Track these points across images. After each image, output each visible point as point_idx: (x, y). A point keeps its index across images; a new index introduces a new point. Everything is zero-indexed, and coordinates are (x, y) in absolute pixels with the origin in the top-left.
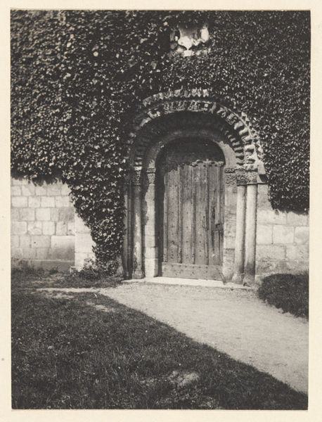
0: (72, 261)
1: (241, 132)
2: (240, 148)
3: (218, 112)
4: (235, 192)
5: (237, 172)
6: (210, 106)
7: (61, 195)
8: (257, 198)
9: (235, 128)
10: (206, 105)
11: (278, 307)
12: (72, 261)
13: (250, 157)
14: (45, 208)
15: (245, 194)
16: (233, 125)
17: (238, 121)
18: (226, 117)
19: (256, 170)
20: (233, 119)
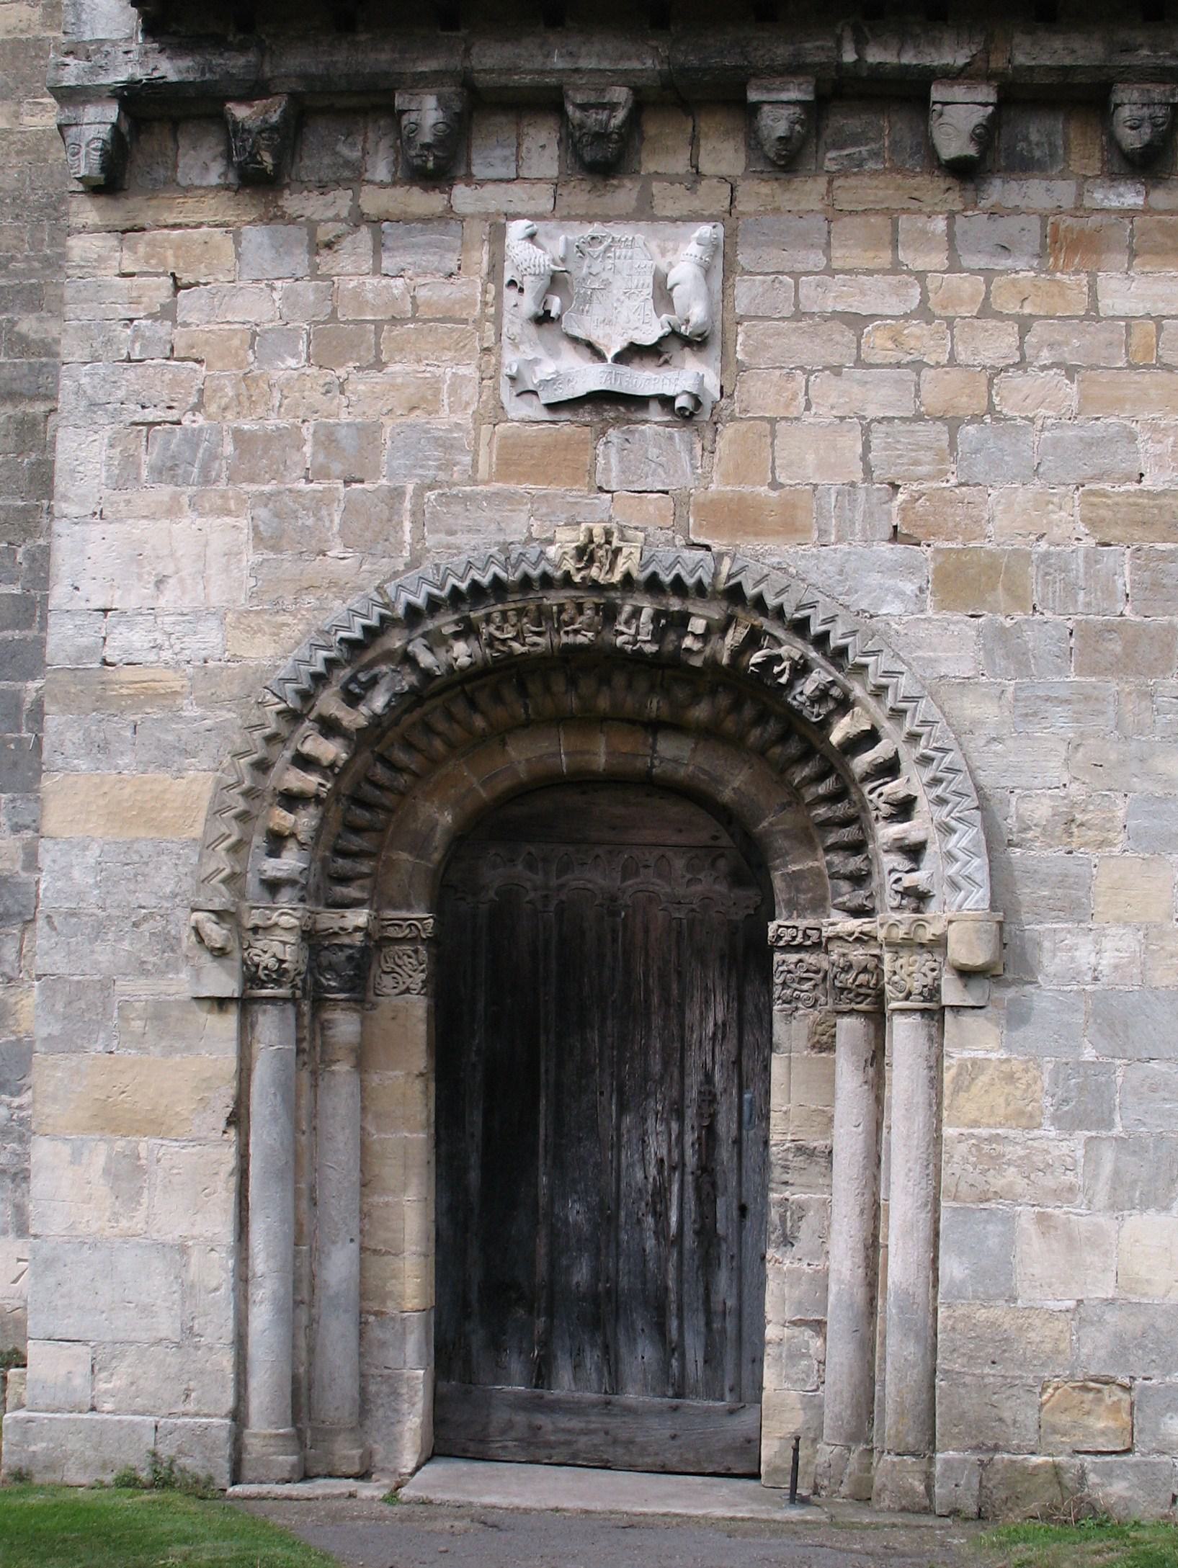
0: (31, 634)
1: (862, 762)
2: (847, 834)
3: (757, 657)
4: (825, 1044)
5: (836, 950)
6: (716, 630)
7: (799, 315)
8: (937, 1140)
9: (836, 737)
10: (698, 625)
11: (1026, 961)
12: (31, 634)
13: (908, 880)
14: (575, 340)
15: (876, 1058)
16: (825, 725)
17: (845, 705)
18: (790, 685)
19: (939, 943)
20: (822, 695)
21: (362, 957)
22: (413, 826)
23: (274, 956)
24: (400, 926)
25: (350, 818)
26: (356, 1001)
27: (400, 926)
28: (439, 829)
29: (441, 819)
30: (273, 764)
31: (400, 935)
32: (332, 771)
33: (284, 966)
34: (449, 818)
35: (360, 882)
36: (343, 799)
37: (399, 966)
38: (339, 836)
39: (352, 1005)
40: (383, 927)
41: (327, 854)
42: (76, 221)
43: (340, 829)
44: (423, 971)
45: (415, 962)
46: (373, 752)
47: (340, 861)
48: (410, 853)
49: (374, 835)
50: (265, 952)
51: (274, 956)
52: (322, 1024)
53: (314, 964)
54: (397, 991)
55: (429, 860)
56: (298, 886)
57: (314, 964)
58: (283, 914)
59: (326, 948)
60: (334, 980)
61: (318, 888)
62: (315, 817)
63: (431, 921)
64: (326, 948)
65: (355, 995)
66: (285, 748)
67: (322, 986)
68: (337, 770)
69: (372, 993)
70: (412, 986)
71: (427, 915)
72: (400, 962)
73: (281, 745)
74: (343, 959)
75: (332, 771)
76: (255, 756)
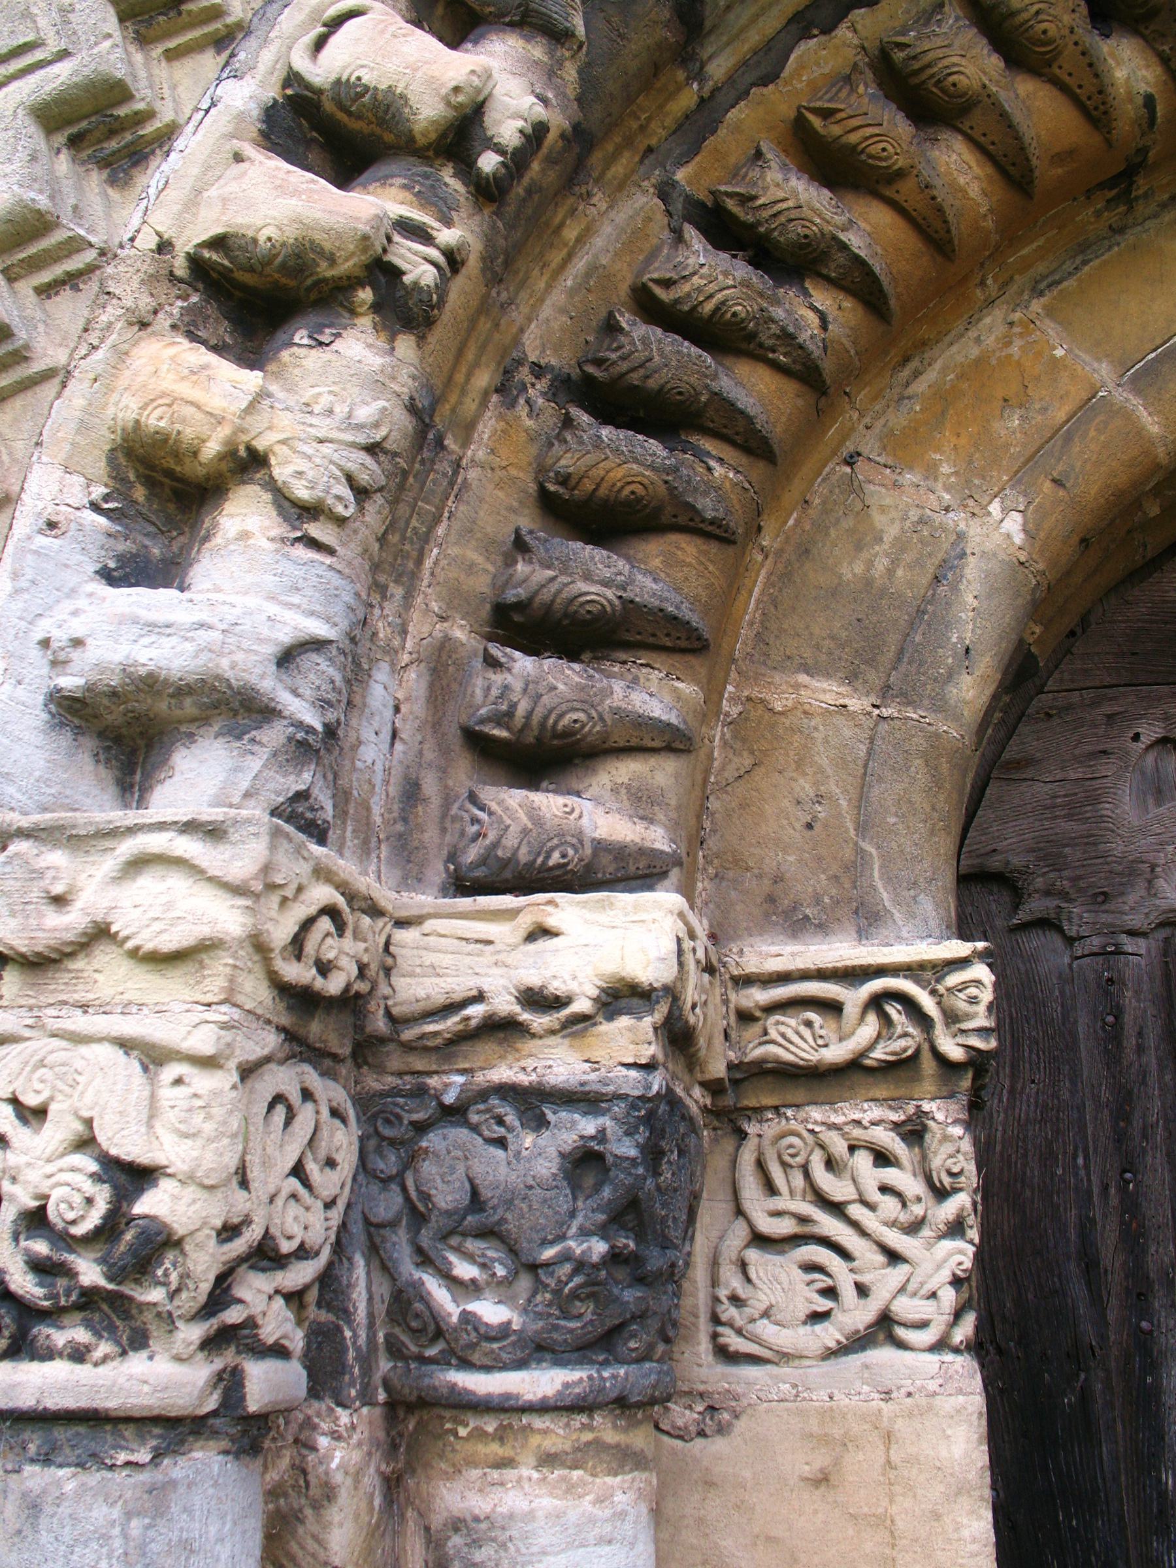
21: (653, 1155)
22: (852, 570)
23: (86, 1142)
24: (833, 1008)
25: (567, 462)
26: (622, 1405)
27: (833, 1008)
28: (972, 569)
29: (974, 531)
30: (169, 134)
31: (836, 1053)
32: (466, 166)
33: (150, 1204)
34: (1013, 525)
35: (626, 770)
36: (537, 391)
37: (836, 1208)
38: (520, 545)
39: (606, 1429)
40: (745, 1017)
41: (460, 633)
42: (297, 340)
43: (526, 521)
44: (956, 1228)
45: (912, 1185)
46: (665, 192)
47: (524, 664)
48: (851, 678)
49: (687, 548)
50: (39, 1114)
51: (86, 1142)
52: (434, 1541)
53: (388, 1204)
54: (829, 1334)
55: (940, 705)
56: (274, 735)
57: (388, 1204)
58: (139, 864)
59: (455, 1113)
60: (503, 1288)
61: (411, 793)
62: (378, 384)
63: (981, 971)
64: (455, 1113)
65: (616, 1375)
66: (230, 71)
67: (433, 1327)
68: (488, 162)
69: (704, 1346)
70: (905, 1308)
71: (959, 948)
72: (836, 1188)
73: (209, 62)
74: (547, 1167)
75: (466, 166)
76: (61, 75)
